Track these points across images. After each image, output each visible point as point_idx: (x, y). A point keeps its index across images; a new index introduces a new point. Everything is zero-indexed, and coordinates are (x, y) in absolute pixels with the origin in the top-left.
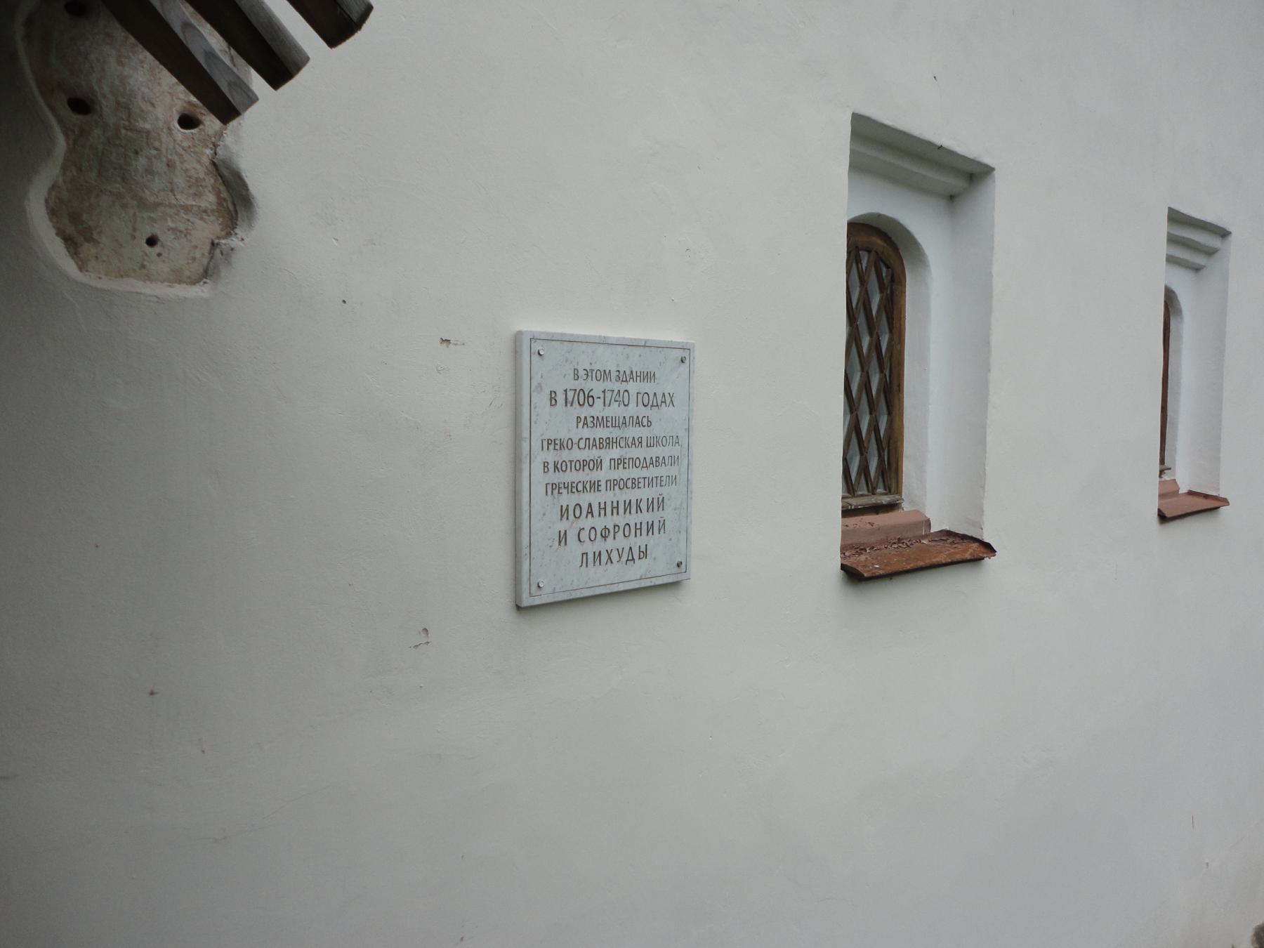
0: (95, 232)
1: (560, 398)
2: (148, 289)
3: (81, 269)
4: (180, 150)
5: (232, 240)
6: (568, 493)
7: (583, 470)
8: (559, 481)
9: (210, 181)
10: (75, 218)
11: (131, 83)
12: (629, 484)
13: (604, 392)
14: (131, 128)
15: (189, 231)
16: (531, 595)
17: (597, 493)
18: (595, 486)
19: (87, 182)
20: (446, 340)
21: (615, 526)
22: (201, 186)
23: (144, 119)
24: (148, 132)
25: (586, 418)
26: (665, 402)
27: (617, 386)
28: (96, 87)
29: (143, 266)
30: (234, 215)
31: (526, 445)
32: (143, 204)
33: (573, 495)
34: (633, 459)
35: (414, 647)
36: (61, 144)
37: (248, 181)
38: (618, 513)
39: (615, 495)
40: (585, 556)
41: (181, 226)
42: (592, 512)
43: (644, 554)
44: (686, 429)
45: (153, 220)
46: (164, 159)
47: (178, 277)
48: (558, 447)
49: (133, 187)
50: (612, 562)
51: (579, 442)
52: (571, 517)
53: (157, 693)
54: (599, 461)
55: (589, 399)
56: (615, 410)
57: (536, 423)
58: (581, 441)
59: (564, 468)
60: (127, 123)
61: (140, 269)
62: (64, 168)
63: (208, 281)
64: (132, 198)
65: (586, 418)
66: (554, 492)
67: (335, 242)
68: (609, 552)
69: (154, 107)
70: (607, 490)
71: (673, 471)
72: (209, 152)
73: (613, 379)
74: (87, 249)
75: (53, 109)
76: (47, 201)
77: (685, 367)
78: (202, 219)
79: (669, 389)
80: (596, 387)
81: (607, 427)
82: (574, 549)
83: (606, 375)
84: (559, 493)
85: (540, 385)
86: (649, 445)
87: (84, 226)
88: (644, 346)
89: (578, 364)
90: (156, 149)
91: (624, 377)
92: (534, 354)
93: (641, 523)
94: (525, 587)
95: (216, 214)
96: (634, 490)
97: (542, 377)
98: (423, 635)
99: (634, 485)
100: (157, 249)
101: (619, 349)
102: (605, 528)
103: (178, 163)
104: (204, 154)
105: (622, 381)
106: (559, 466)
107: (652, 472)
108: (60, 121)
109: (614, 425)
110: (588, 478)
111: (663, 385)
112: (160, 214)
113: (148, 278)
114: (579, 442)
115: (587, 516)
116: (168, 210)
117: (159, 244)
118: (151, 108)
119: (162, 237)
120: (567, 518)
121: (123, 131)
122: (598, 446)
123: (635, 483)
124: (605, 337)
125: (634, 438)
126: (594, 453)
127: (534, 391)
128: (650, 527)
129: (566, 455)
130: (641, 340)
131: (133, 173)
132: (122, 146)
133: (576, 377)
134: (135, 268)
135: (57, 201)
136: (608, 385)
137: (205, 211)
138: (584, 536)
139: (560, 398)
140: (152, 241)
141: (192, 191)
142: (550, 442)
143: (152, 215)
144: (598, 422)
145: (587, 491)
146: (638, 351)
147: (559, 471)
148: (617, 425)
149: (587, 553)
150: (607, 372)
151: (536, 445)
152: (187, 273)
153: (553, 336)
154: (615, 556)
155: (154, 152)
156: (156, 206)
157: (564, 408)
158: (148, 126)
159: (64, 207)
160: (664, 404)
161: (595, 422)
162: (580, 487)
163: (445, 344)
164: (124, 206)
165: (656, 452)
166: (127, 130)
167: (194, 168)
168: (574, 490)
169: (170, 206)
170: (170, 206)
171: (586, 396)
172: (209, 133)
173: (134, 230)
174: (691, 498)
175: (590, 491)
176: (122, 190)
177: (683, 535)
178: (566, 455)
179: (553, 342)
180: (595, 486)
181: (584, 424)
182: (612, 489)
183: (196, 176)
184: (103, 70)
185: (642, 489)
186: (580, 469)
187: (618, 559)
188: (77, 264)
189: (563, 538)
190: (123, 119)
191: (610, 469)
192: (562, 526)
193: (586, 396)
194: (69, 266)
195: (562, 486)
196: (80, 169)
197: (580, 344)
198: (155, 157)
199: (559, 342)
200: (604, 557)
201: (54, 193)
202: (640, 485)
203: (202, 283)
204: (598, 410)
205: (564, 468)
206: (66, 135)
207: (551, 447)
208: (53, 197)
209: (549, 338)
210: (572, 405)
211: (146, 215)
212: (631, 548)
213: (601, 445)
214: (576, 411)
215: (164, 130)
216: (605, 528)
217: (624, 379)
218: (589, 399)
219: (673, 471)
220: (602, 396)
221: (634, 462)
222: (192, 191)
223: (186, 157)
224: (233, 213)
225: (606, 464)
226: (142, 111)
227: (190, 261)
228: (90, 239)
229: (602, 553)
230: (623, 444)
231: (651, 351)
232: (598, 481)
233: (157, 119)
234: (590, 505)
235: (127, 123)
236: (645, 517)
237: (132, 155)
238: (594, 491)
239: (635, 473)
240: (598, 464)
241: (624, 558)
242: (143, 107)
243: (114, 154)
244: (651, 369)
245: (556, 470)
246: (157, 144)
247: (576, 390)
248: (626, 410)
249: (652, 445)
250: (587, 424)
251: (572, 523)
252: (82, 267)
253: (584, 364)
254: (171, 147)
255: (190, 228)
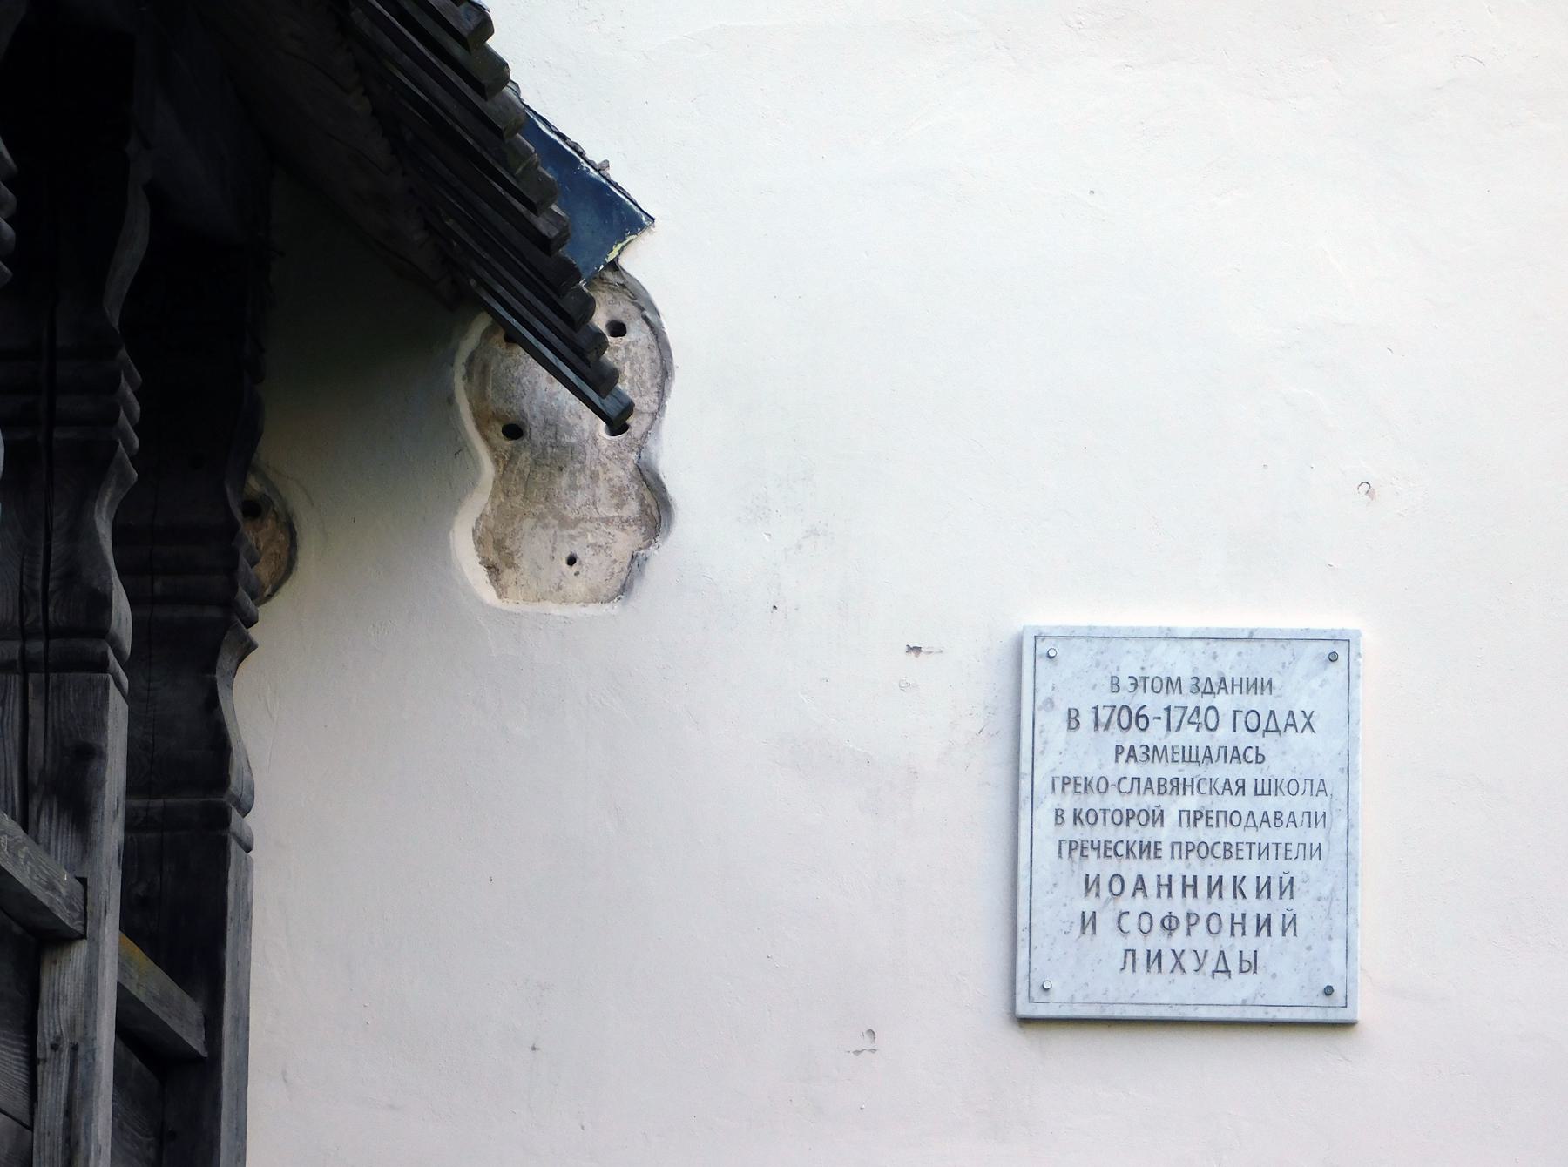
0: (515, 557)
1: (1087, 719)
2: (555, 609)
3: (500, 596)
4: (604, 459)
5: (231, 661)
6: (1099, 856)
7: (1128, 825)
8: (1084, 838)
9: (633, 488)
10: (499, 545)
11: (560, 398)
12: (1219, 851)
13: (1168, 709)
14: (556, 445)
15: (609, 545)
16: (1030, 999)
17: (1154, 862)
18: (1149, 850)
19: (512, 507)
20: (915, 648)
21: (1189, 915)
22: (625, 494)
23: (570, 435)
24: (573, 447)
25: (1132, 748)
26: (1294, 725)
27: (1191, 701)
28: (526, 410)
29: (560, 588)
30: (658, 522)
31: (1025, 785)
32: (564, 522)
33: (1108, 861)
34: (1226, 812)
35: (854, 1052)
36: (488, 470)
37: (666, 482)
38: (1195, 895)
39: (1188, 866)
40: (1130, 955)
41: (601, 541)
42: (1143, 888)
43: (1251, 965)
44: (1342, 770)
45: (572, 537)
46: (588, 472)
47: (595, 597)
48: (1081, 789)
49: (556, 505)
50: (1184, 971)
51: (1119, 783)
52: (1105, 893)
53: (538, 1049)
54: (1158, 812)
55: (1139, 719)
56: (1190, 736)
57: (1042, 752)
58: (1123, 781)
59: (1092, 820)
60: (553, 441)
61: (556, 590)
62: (493, 496)
63: (622, 597)
64: (554, 518)
65: (1132, 748)
66: (1073, 854)
67: (767, 538)
68: (1201, 956)
69: (580, 418)
70: (1173, 857)
71: (1315, 836)
72: (633, 456)
73: (1186, 690)
74: (508, 576)
75: (486, 438)
76: (474, 531)
77: (1336, 672)
78: (623, 530)
79: (1301, 704)
80: (1153, 703)
81: (1173, 761)
82: (1109, 944)
83: (1172, 684)
84: (1082, 855)
85: (1050, 702)
86: (1259, 791)
87: (507, 551)
88: (1249, 639)
89: (1118, 669)
90: (581, 462)
91: (1204, 687)
92: (1041, 656)
93: (1244, 915)
94: (1022, 987)
95: (639, 523)
96: (1227, 862)
97: (1053, 689)
98: (868, 1038)
99: (1228, 854)
100: (575, 568)
101: (1199, 645)
102: (1170, 915)
103: (601, 473)
104: (627, 459)
105: (1204, 693)
106: (1083, 816)
107: (1266, 835)
108: (492, 448)
109: (1187, 759)
110: (1137, 838)
111: (1295, 694)
112: (581, 531)
113: (565, 600)
114: (1119, 783)
115: (1134, 895)
116: (589, 525)
117: (577, 562)
118: (577, 421)
119: (580, 556)
120: (1097, 895)
121: (549, 450)
122: (1156, 790)
123: (1229, 851)
124: (1169, 629)
125: (1227, 780)
126: (1149, 800)
127: (1040, 708)
128: (1264, 924)
129: (1094, 801)
130: (1243, 630)
131: (557, 491)
132: (547, 466)
133: (1115, 686)
134: (552, 589)
135: (485, 530)
136: (1175, 699)
137: (627, 521)
138: (1129, 923)
139: (1087, 719)
140: (572, 561)
141: (615, 501)
142: (1066, 781)
143: (573, 532)
144: (1153, 754)
145: (1135, 857)
146: (1234, 648)
147: (1082, 823)
148: (1194, 759)
149: (1134, 951)
150: (1174, 680)
151: (1042, 784)
152: (604, 591)
153: (1119, 631)
154: (1189, 962)
155: (578, 466)
156: (578, 521)
157: (1093, 733)
158: (573, 440)
159: (490, 535)
160: (1291, 730)
161: (1150, 754)
162: (1122, 849)
163: (913, 654)
164: (545, 527)
165: (1271, 804)
166: (553, 447)
167: (617, 476)
168: (1110, 853)
169: (591, 520)
170: (591, 520)
171: (1134, 715)
172: (636, 436)
173: (554, 549)
174: (1357, 884)
175: (1141, 857)
176: (545, 510)
177: (1338, 945)
178: (1094, 801)
179: (1074, 640)
180: (1149, 850)
181: (1129, 756)
182: (1184, 856)
183: (619, 484)
184: (534, 390)
185: (1246, 862)
186: (1121, 823)
187: (1196, 966)
188: (497, 592)
189: (1088, 922)
190: (550, 437)
191: (1180, 825)
192: (1089, 905)
193: (1134, 715)
194: (488, 594)
195: (1089, 845)
196: (507, 495)
197: (1123, 640)
198: (579, 471)
199: (1084, 640)
200: (1168, 961)
201: (482, 522)
202: (1241, 854)
203: (615, 600)
204: (1156, 735)
205: (1092, 820)
206: (496, 462)
207: (1070, 788)
208: (481, 526)
209: (1067, 635)
210: (1107, 727)
211: (566, 533)
212: (1222, 953)
213: (1175, 784)
214: (1115, 737)
215: (589, 441)
216: (1170, 915)
217: (1208, 690)
218: (1139, 719)
219: (1315, 836)
220: (1164, 715)
221: (1230, 818)
222: (615, 501)
223: (610, 465)
224: (658, 520)
225: (1171, 817)
226: (568, 425)
227: (608, 578)
228: (511, 565)
229: (1163, 953)
230: (1205, 788)
231: (1263, 646)
232: (1156, 843)
233: (583, 430)
234: (1140, 878)
235: (553, 441)
236: (1254, 906)
237: (557, 474)
238: (1149, 857)
239: (1229, 835)
240: (1157, 817)
241: (1210, 965)
242: (570, 421)
243: (539, 475)
244: (1264, 674)
245: (1078, 822)
246: (581, 457)
247: (1115, 707)
248: (1212, 737)
249: (1266, 792)
250: (1135, 757)
251: (1107, 902)
252: (502, 593)
253: (1129, 667)
254: (595, 457)
255: (611, 541)
